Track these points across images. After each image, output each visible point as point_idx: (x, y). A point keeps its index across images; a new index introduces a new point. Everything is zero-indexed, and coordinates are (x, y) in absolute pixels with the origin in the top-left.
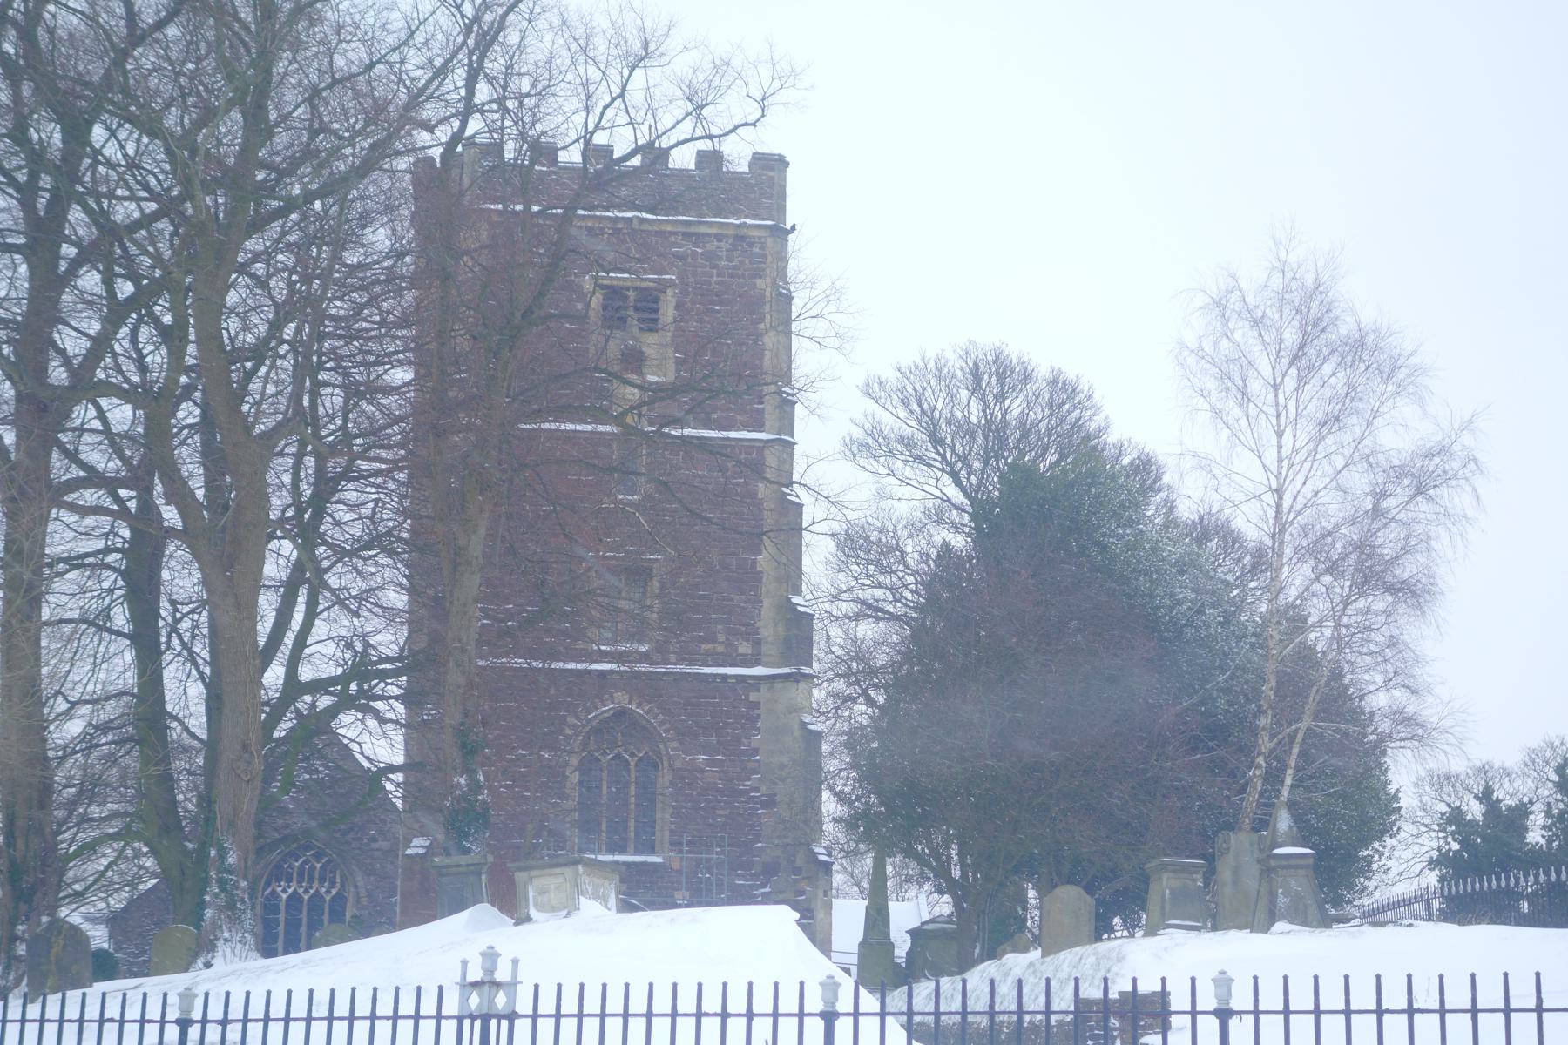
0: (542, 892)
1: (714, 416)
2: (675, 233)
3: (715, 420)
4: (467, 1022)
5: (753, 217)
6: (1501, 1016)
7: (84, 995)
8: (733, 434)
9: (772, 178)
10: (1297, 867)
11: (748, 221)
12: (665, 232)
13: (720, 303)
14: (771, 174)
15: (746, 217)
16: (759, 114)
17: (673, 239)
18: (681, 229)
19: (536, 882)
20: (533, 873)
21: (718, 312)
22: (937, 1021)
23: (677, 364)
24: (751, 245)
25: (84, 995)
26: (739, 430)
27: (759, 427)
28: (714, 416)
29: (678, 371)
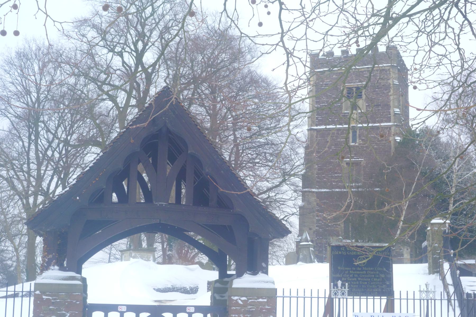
0: (125, 257)
1: (377, 120)
2: (365, 71)
3: (377, 121)
4: (422, 301)
5: (386, 64)
6: (413, 300)
7: (31, 284)
8: (382, 124)
9: (392, 52)
10: (305, 248)
11: (385, 65)
12: (362, 71)
13: (378, 89)
14: (391, 51)
15: (384, 64)
16: (86, 39)
17: (365, 72)
18: (366, 69)
19: (125, 254)
20: (123, 252)
21: (377, 91)
22: (15, 293)
23: (366, 107)
24: (386, 71)
25: (31, 284)
26: (384, 123)
27: (390, 122)
28: (377, 120)
29: (367, 108)
